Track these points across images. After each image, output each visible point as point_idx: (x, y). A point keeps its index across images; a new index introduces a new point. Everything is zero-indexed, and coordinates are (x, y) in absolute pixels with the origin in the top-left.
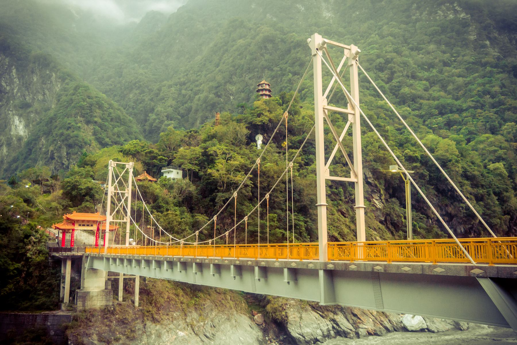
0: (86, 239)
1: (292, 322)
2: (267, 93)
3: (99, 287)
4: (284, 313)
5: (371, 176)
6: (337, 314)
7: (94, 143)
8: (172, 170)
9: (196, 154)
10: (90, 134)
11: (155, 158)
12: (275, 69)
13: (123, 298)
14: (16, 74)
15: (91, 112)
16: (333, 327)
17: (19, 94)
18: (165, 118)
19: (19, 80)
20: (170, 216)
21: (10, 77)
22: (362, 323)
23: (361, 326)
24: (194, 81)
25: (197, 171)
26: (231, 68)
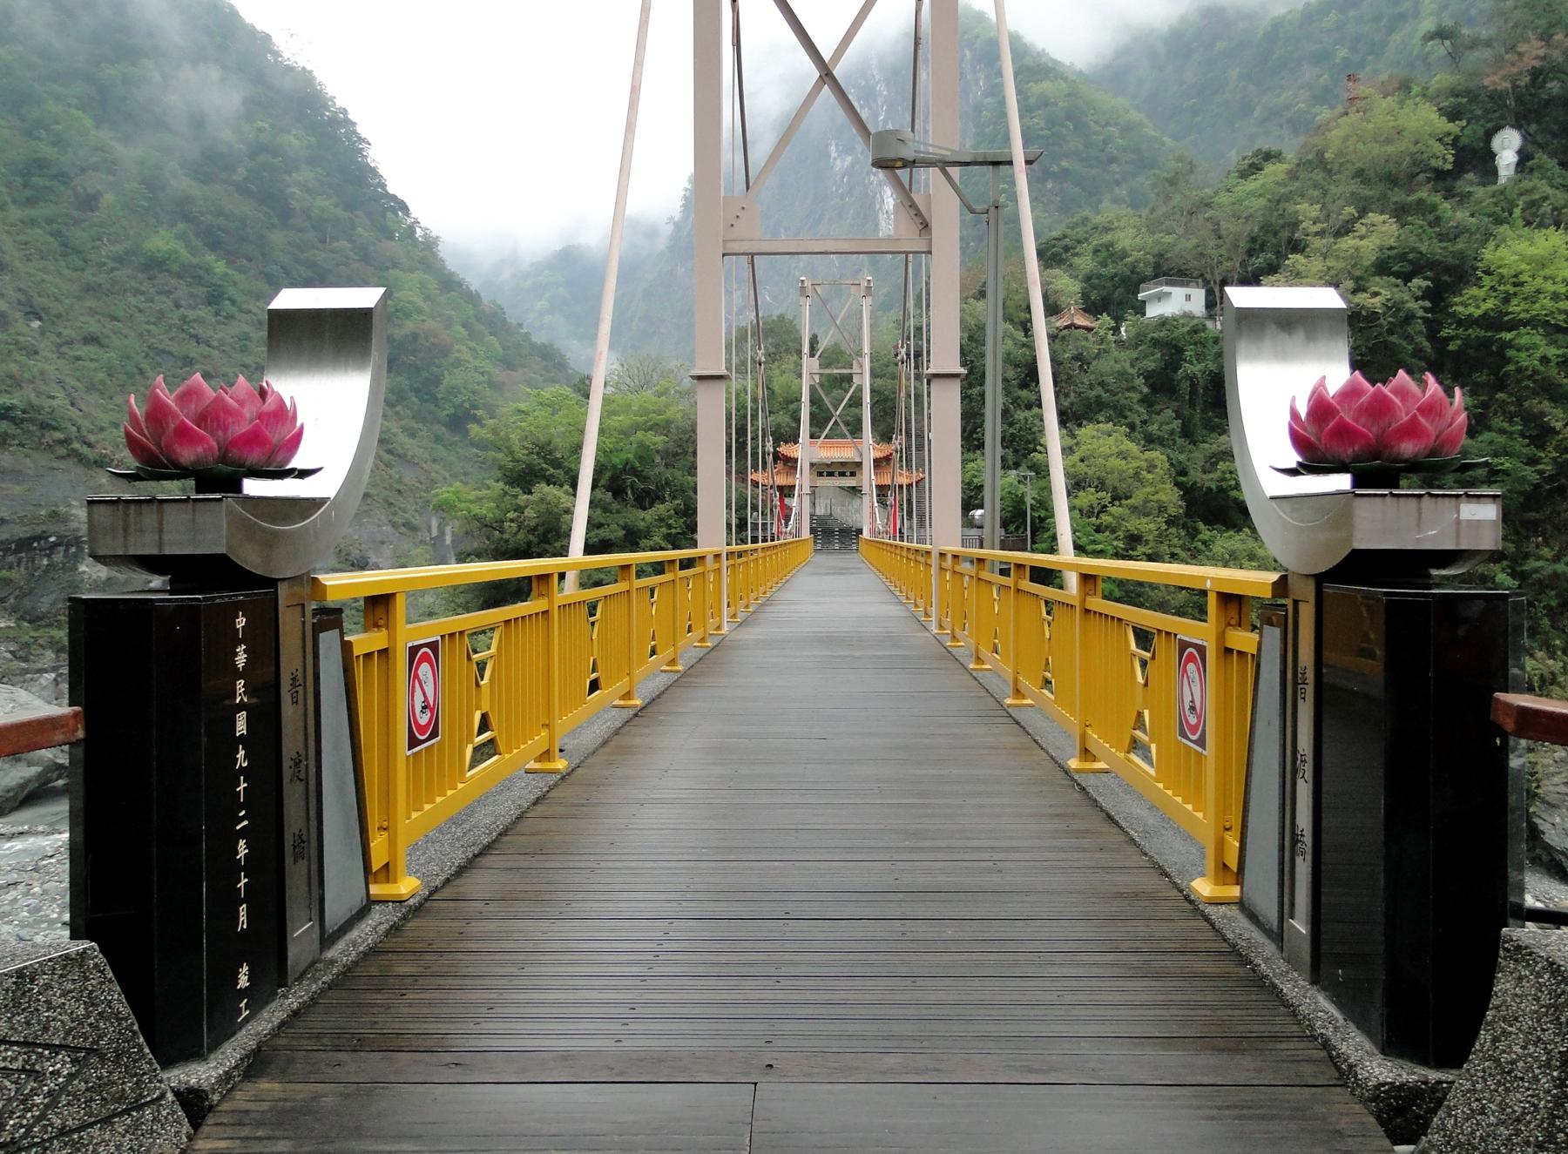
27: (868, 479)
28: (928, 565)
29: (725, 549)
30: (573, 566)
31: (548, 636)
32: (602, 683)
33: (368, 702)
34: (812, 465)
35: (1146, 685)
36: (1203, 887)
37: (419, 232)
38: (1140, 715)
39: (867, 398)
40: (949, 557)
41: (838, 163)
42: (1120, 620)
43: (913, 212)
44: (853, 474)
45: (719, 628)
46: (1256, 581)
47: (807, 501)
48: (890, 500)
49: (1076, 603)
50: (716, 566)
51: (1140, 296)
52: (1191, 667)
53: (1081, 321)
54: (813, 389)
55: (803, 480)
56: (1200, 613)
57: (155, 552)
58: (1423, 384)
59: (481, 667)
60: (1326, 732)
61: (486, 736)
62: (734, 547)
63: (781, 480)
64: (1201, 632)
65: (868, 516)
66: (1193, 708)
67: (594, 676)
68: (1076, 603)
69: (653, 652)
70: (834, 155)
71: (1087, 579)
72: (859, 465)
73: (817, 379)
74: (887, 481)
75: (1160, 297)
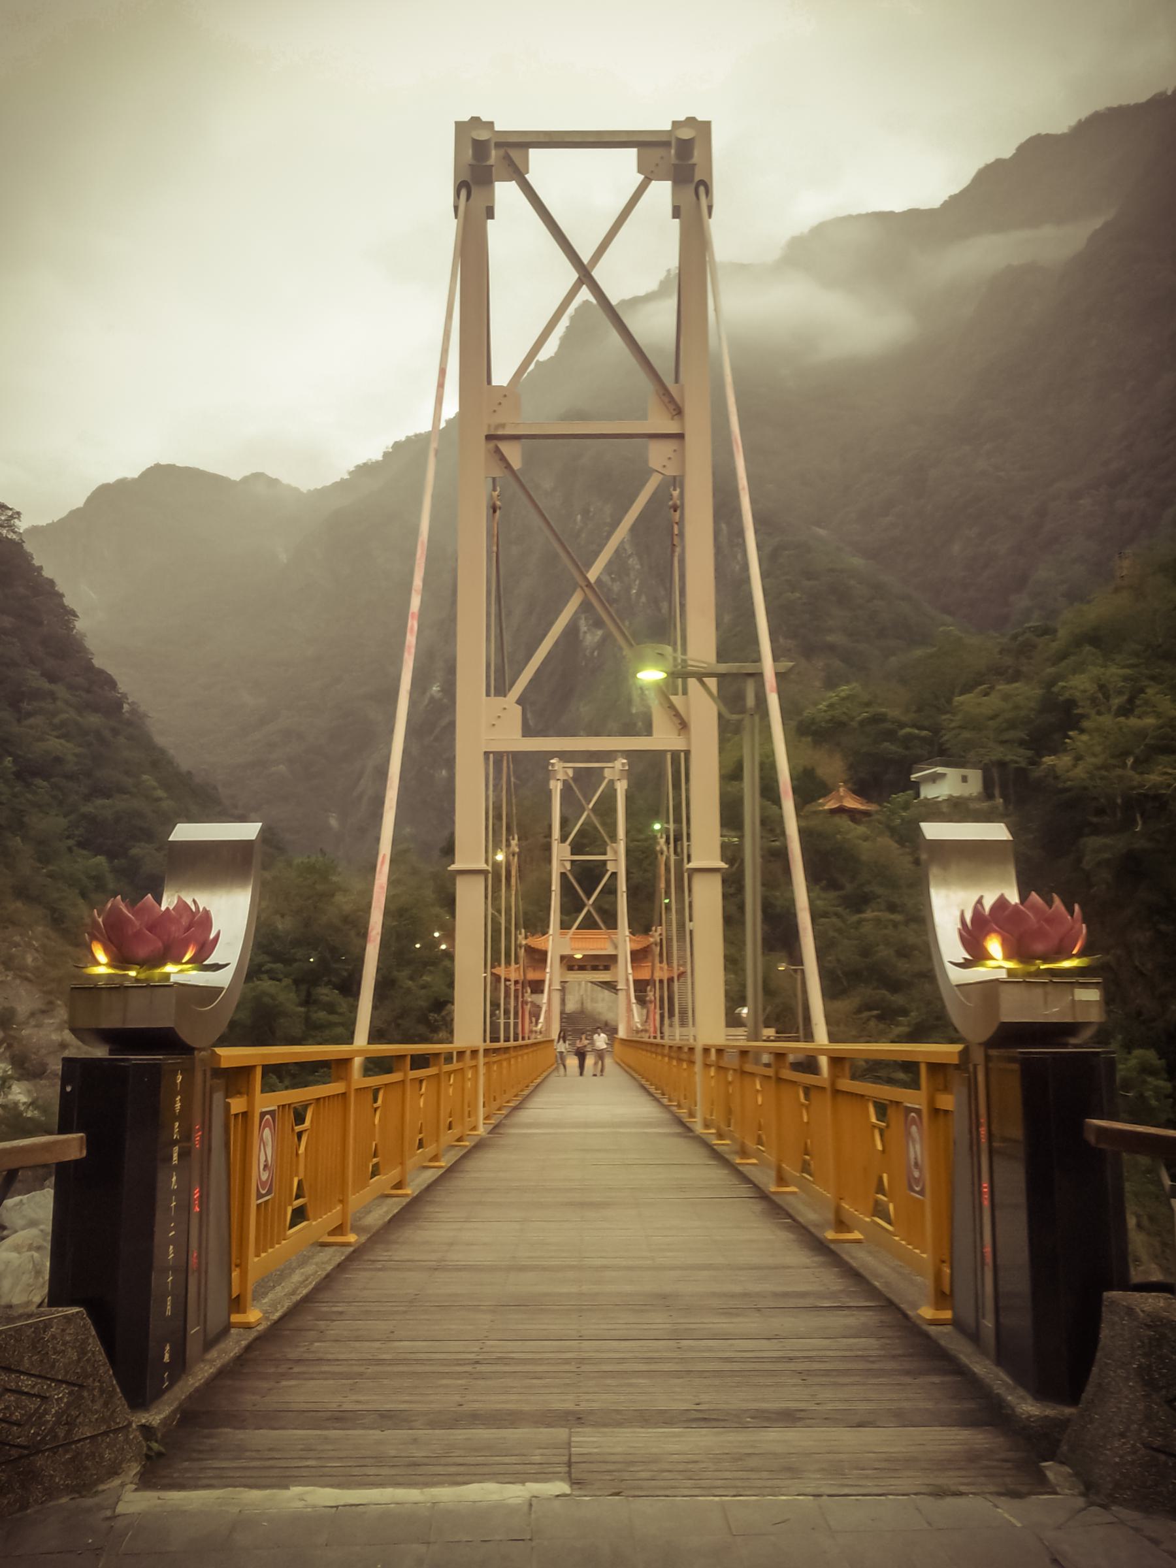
8: (940, 770)
9: (1017, 707)
10: (818, 684)
11: (890, 735)
17: (643, 599)
20: (867, 928)
25: (1023, 764)
27: (625, 973)
28: (692, 1062)
29: (481, 1046)
30: (359, 1052)
31: (404, 1093)
32: (310, 1212)
33: (235, 1150)
34: (562, 958)
35: (883, 1151)
36: (927, 1312)
37: (126, 707)
38: (881, 1179)
39: (622, 886)
40: (713, 1051)
41: (589, 637)
42: (862, 1096)
43: (666, 400)
44: (607, 968)
45: (474, 1128)
46: (947, 1051)
47: (556, 997)
48: (650, 995)
49: (827, 1085)
50: (473, 1063)
51: (914, 777)
52: (914, 1129)
53: (851, 803)
54: (563, 875)
55: (552, 973)
56: (915, 1084)
57: (118, 1025)
58: (1050, 903)
59: (300, 1135)
60: (995, 1167)
61: (300, 1202)
62: (489, 1045)
63: (532, 975)
64: (915, 1099)
65: (628, 1016)
66: (916, 1164)
67: (375, 1160)
68: (827, 1085)
69: (421, 1145)
70: (583, 628)
71: (837, 1061)
72: (613, 958)
73: (568, 866)
74: (645, 975)
75: (935, 778)
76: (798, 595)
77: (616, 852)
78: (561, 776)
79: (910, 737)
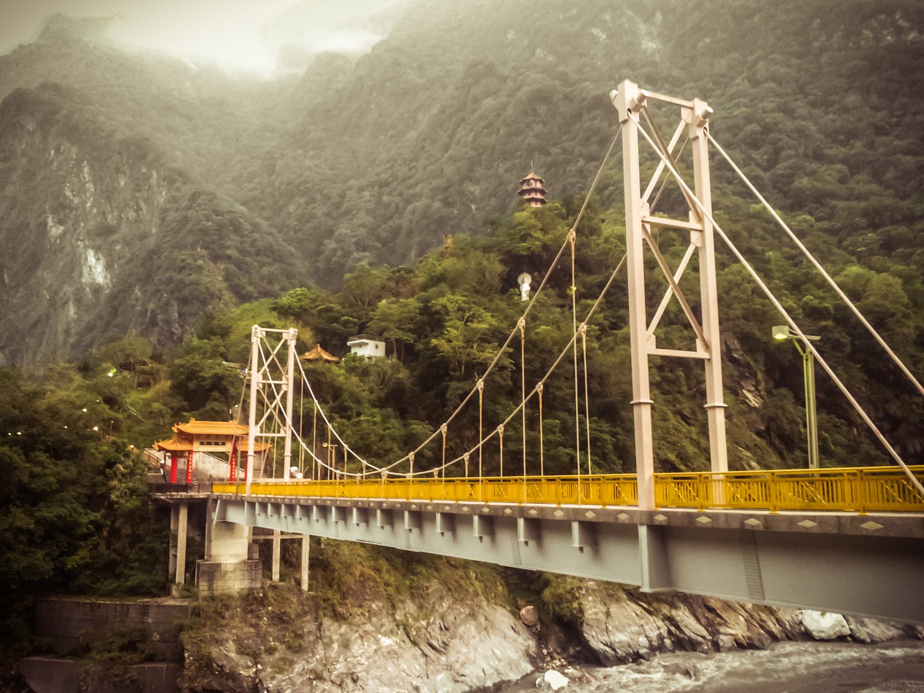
0: (213, 468)
1: (591, 622)
2: (539, 196)
3: (236, 555)
4: (575, 605)
5: (738, 346)
6: (676, 608)
7: (227, 296)
8: (365, 341)
10: (220, 278)
11: (336, 320)
12: (554, 150)
13: (281, 576)
14: (90, 174)
15: (222, 239)
16: (670, 632)
17: (95, 211)
18: (353, 247)
19: (95, 185)
21: (80, 181)
22: (725, 623)
23: (722, 629)
24: (405, 179)
25: (412, 342)
26: (472, 153)
41: (54, 230)
51: (348, 343)
73: (261, 386)
76: (210, 224)
77: (287, 379)
78: (259, 335)
79: (348, 322)
